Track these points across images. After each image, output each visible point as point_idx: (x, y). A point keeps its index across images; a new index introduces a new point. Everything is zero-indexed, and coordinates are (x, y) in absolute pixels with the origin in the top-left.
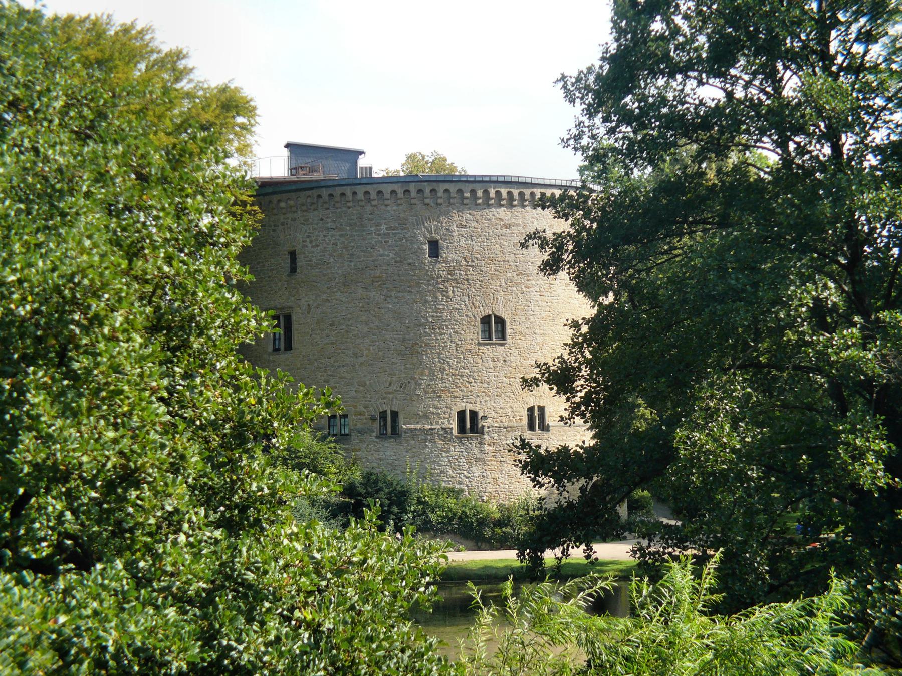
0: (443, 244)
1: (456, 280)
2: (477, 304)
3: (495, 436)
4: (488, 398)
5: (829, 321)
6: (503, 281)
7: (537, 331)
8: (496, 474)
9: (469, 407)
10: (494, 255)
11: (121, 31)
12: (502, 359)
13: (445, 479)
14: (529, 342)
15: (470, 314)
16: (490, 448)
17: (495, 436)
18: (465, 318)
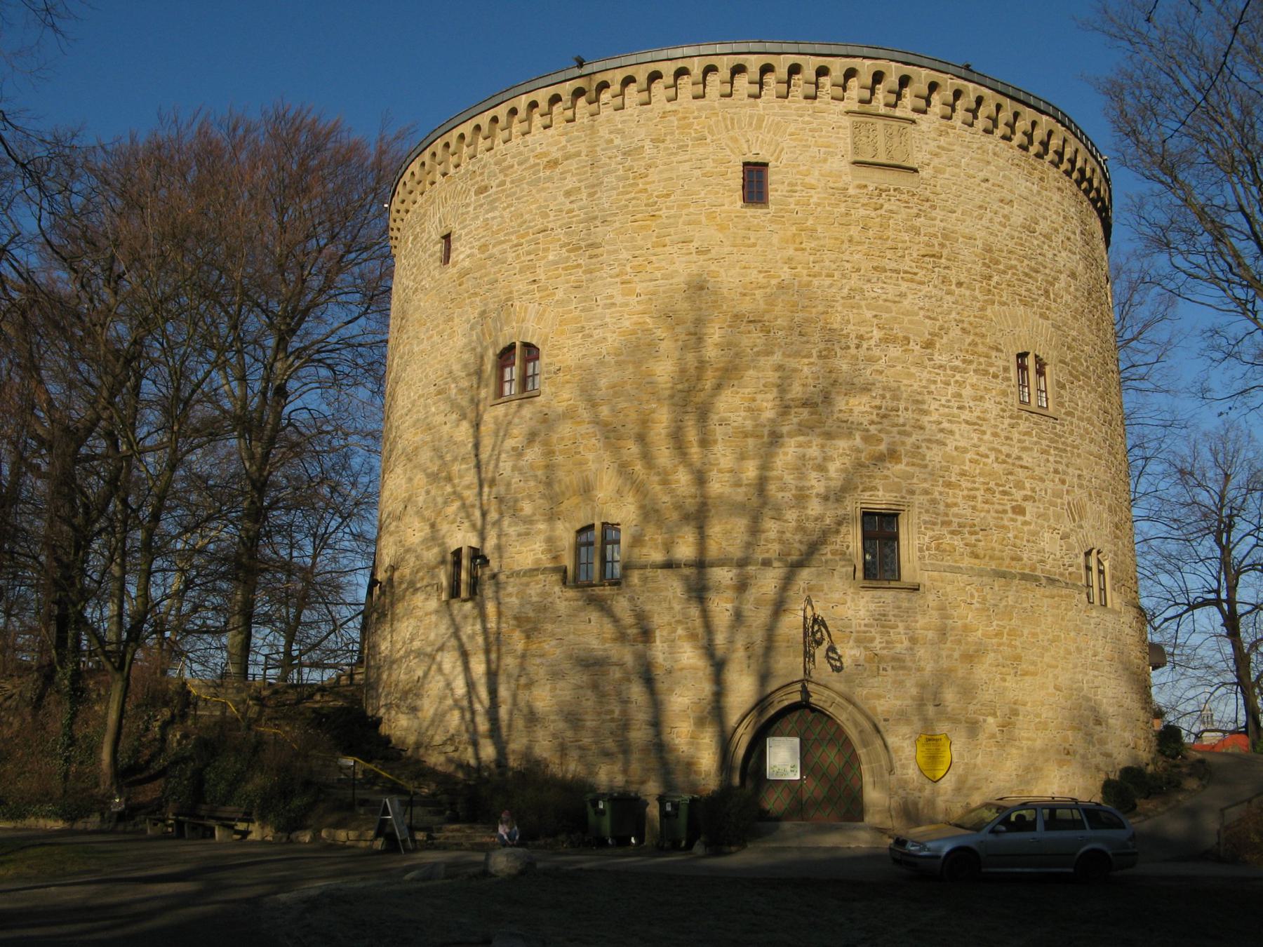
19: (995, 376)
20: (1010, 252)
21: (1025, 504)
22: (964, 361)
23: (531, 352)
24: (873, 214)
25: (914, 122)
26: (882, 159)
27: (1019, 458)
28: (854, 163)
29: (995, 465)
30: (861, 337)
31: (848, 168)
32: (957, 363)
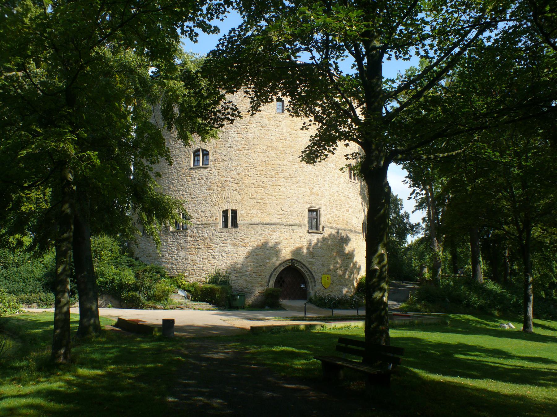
4: (194, 205)
5: (314, 412)
7: (234, 158)
8: (194, 258)
12: (205, 177)
13: (164, 261)
14: (226, 166)
16: (191, 239)
32: (334, 167)
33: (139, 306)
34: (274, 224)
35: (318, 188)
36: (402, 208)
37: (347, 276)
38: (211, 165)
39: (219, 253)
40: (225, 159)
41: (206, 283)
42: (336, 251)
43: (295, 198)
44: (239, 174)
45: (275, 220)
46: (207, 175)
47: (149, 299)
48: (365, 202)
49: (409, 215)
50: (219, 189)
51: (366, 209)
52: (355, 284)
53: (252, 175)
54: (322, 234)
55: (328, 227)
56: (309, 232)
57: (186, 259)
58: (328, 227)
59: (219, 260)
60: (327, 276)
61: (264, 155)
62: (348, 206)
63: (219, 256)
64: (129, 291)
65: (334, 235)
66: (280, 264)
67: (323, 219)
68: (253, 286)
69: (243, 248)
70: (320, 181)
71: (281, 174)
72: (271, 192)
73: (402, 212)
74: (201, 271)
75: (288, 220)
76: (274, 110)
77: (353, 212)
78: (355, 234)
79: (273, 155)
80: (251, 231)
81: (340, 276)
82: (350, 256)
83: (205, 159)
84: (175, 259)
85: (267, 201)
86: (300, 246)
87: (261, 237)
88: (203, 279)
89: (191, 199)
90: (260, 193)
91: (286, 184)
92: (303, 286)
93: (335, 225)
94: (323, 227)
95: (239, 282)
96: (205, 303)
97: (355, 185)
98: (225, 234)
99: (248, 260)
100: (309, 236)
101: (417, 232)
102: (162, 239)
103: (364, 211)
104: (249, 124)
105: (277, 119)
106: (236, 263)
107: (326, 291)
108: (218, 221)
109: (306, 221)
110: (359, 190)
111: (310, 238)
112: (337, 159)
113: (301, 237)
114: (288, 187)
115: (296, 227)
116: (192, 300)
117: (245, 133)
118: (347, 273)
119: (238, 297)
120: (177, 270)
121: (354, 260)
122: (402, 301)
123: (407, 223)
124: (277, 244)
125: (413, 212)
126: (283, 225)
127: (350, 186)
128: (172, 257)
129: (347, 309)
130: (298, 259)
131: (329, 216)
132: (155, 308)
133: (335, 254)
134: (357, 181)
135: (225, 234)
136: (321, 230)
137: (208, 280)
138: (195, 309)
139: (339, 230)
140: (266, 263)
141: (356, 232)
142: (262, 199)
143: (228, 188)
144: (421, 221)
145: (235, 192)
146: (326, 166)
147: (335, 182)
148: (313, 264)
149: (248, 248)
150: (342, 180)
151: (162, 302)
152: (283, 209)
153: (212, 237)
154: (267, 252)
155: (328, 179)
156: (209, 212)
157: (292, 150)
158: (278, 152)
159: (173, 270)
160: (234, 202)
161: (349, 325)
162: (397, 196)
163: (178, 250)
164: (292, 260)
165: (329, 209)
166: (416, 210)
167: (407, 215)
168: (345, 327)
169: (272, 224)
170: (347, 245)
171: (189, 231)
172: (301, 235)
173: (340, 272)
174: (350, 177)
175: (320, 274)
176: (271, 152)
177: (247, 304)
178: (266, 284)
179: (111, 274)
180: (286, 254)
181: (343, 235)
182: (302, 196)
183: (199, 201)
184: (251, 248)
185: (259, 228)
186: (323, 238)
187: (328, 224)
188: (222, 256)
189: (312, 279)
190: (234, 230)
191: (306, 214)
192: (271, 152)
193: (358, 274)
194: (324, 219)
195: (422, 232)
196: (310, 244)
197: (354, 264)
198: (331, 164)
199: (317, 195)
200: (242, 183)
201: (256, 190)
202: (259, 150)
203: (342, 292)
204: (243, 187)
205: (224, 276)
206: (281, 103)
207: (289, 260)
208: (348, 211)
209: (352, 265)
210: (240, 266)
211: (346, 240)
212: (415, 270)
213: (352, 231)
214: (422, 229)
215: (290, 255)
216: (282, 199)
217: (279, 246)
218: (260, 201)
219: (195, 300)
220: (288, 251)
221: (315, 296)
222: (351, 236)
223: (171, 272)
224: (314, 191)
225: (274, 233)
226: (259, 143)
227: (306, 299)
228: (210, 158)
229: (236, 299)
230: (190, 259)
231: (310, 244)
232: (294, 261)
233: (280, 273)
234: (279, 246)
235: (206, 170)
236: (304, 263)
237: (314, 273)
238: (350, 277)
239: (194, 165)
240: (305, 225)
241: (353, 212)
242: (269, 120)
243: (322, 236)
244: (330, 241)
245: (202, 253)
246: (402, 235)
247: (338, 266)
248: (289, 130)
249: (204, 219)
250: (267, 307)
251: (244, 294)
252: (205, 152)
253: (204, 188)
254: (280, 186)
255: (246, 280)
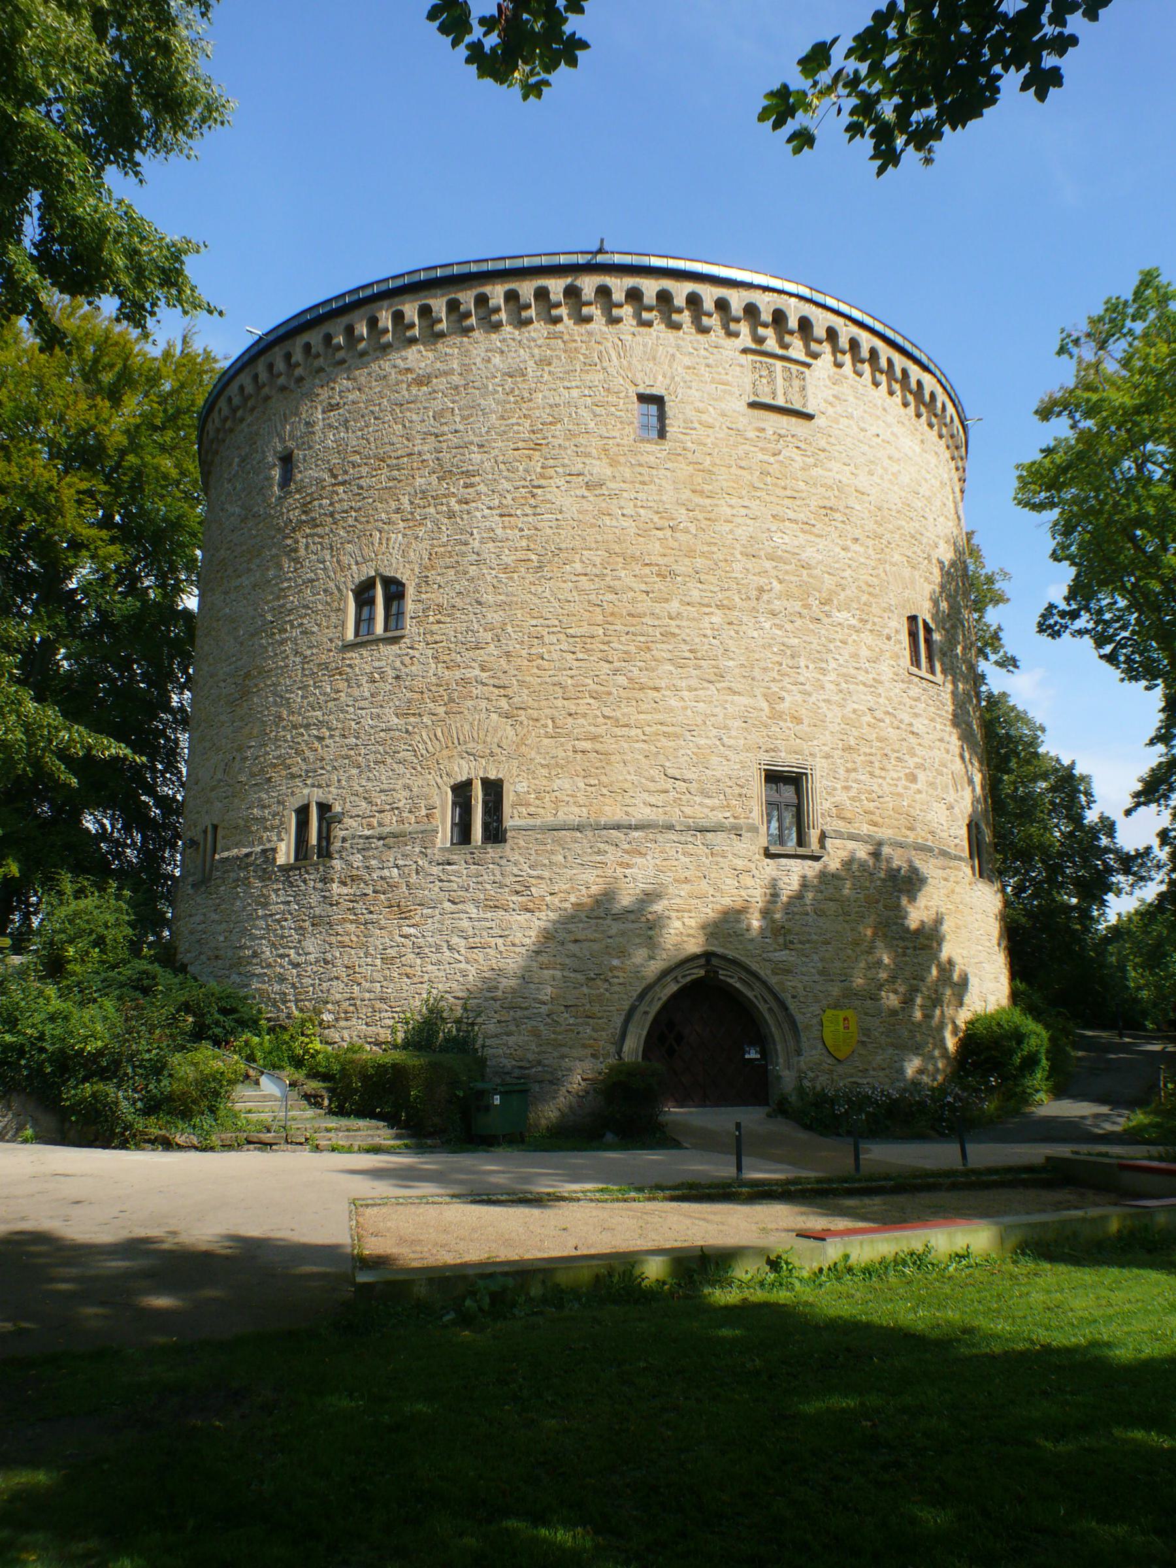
0: (299, 454)
1: (314, 519)
2: (345, 560)
3: (357, 859)
4: (355, 771)
6: (405, 500)
7: (490, 598)
8: (354, 956)
9: (317, 795)
10: (388, 448)
11: (1019, 712)
13: (259, 971)
14: (462, 627)
15: (332, 584)
16: (345, 890)
17: (357, 859)
18: (322, 596)
19: (889, 638)
20: (898, 512)
21: (916, 771)
22: (861, 620)
23: (395, 591)
24: (772, 460)
25: (808, 366)
26: (780, 402)
27: (911, 725)
28: (753, 405)
29: (890, 730)
30: (761, 590)
31: (743, 407)
32: (854, 622)
33: (113, 1135)
34: (637, 828)
35: (799, 698)
36: (1089, 802)
37: (918, 1015)
38: (410, 627)
39: (437, 939)
40: (460, 605)
41: (395, 1047)
42: (871, 920)
43: (714, 732)
44: (508, 654)
45: (642, 813)
46: (398, 664)
47: (152, 1107)
48: (972, 746)
49: (1113, 824)
50: (441, 710)
51: (978, 778)
52: (951, 1043)
53: (555, 656)
54: (817, 858)
55: (839, 835)
56: (768, 854)
57: (326, 962)
58: (839, 835)
59: (439, 962)
60: (842, 1014)
61: (598, 583)
62: (911, 762)
63: (438, 948)
64: (85, 1079)
65: (863, 865)
66: (665, 973)
67: (822, 802)
68: (563, 1057)
69: (523, 918)
70: (803, 670)
71: (661, 650)
72: (626, 711)
73: (1091, 817)
74: (379, 1005)
75: (688, 811)
76: (628, 429)
77: (932, 784)
78: (941, 861)
79: (630, 581)
80: (552, 852)
81: (893, 1013)
82: (927, 940)
83: (394, 610)
84: (291, 963)
85: (610, 745)
86: (738, 905)
87: (590, 876)
88: (385, 1035)
89: (345, 751)
90: (585, 715)
91: (679, 683)
92: (753, 1054)
93: (865, 829)
94: (823, 836)
95: (511, 1040)
96: (374, 1123)
97: (933, 690)
98: (460, 867)
99: (543, 959)
100: (770, 868)
101: (1142, 879)
102: (251, 895)
103: (971, 781)
104: (542, 482)
105: (643, 459)
106: (500, 972)
107: (840, 1069)
108: (437, 822)
109: (756, 812)
110: (950, 708)
111: (775, 873)
112: (864, 598)
113: (738, 873)
114: (685, 694)
115: (721, 836)
116: (331, 1112)
117: (529, 511)
118: (919, 1001)
119: (497, 1100)
120: (297, 1001)
121: (944, 955)
122: (1133, 1104)
123: (1107, 850)
124: (649, 897)
125: (1128, 813)
126: (670, 827)
127: (915, 691)
128: (281, 956)
129: (921, 1137)
130: (731, 954)
131: (842, 797)
132: (168, 1145)
133: (869, 932)
134: (939, 678)
135: (460, 867)
136: (814, 845)
137: (400, 1036)
138: (317, 1148)
139: (880, 844)
140: (612, 969)
141: (944, 854)
142: (594, 738)
143: (470, 703)
144: (1155, 842)
145: (494, 716)
146: (825, 620)
147: (862, 677)
148: (789, 971)
149: (542, 915)
150: (886, 669)
151: (196, 1120)
152: (670, 772)
153: (413, 879)
154: (615, 928)
155: (833, 665)
156: (407, 793)
157: (700, 562)
158: (647, 570)
159: (285, 1002)
160: (492, 754)
161: (919, 1247)
162: (1072, 766)
163: (300, 930)
164: (708, 956)
165: (841, 771)
166: (1138, 805)
167: (1108, 827)
168: (899, 1262)
169: (630, 827)
170: (913, 899)
171: (337, 864)
172: (740, 863)
173: (892, 1000)
174: (916, 662)
175: (816, 1009)
176: (623, 574)
177: (543, 1122)
178: (612, 1049)
179: (38, 1017)
180: (683, 932)
181: (896, 863)
182: (738, 723)
183: (371, 757)
184: (553, 916)
185: (581, 843)
186: (823, 875)
187: (841, 825)
188: (450, 948)
189: (786, 1026)
190: (492, 851)
191: (757, 788)
192: (623, 574)
193: (961, 1004)
194: (827, 805)
195: (1160, 876)
196: (775, 895)
197: (941, 969)
198: (845, 614)
199: (798, 720)
200: (521, 683)
201: (571, 706)
202: (578, 567)
203: (901, 1071)
204: (524, 697)
205: (458, 1021)
206: (653, 409)
207: (695, 957)
208: (913, 778)
209: (934, 972)
210: (513, 983)
211: (909, 883)
212: (1137, 1001)
213: (930, 850)
214: (1159, 867)
215: (701, 940)
216: (666, 735)
217: (658, 907)
218: (587, 745)
219: (340, 1111)
220: (692, 922)
221: (801, 1090)
222: (928, 867)
223: (279, 1010)
224: (784, 706)
225: (639, 860)
226: (577, 543)
227: (767, 1104)
228: (410, 606)
229: (488, 1108)
230: (339, 962)
231: (775, 895)
232: (715, 961)
233: (664, 1008)
234: (658, 907)
235: (395, 647)
236: (754, 967)
237: (792, 1005)
238: (928, 1017)
239: (357, 634)
240: (754, 829)
241: (932, 784)
242: (613, 463)
243: (817, 866)
244: (848, 884)
245: (379, 939)
246: (1096, 888)
247: (883, 975)
248: (686, 494)
249: (387, 817)
250: (609, 1137)
251: (523, 1087)
252: (393, 588)
253: (389, 711)
254: (656, 689)
255: (535, 1033)
